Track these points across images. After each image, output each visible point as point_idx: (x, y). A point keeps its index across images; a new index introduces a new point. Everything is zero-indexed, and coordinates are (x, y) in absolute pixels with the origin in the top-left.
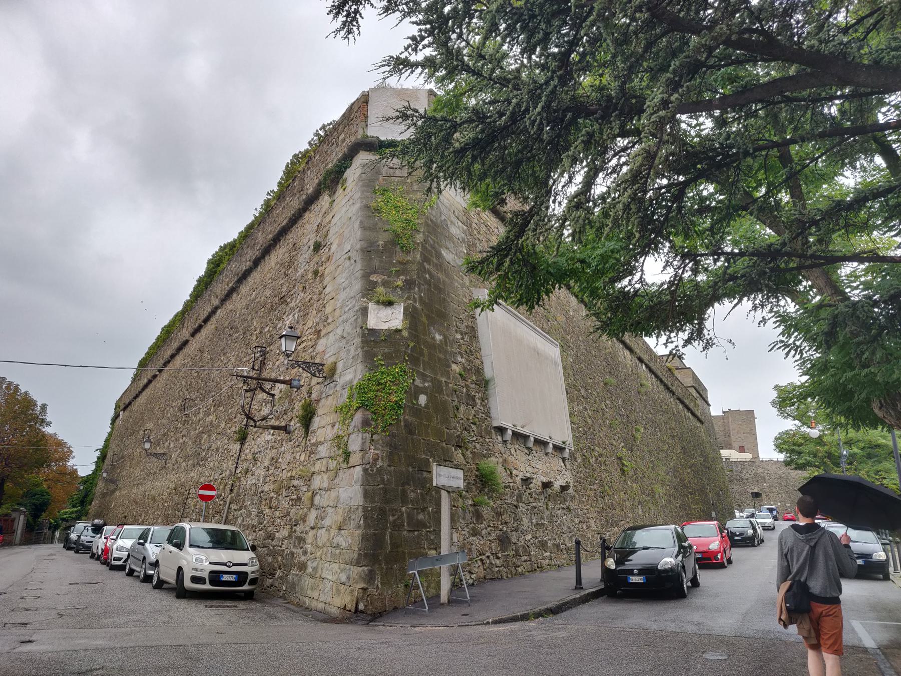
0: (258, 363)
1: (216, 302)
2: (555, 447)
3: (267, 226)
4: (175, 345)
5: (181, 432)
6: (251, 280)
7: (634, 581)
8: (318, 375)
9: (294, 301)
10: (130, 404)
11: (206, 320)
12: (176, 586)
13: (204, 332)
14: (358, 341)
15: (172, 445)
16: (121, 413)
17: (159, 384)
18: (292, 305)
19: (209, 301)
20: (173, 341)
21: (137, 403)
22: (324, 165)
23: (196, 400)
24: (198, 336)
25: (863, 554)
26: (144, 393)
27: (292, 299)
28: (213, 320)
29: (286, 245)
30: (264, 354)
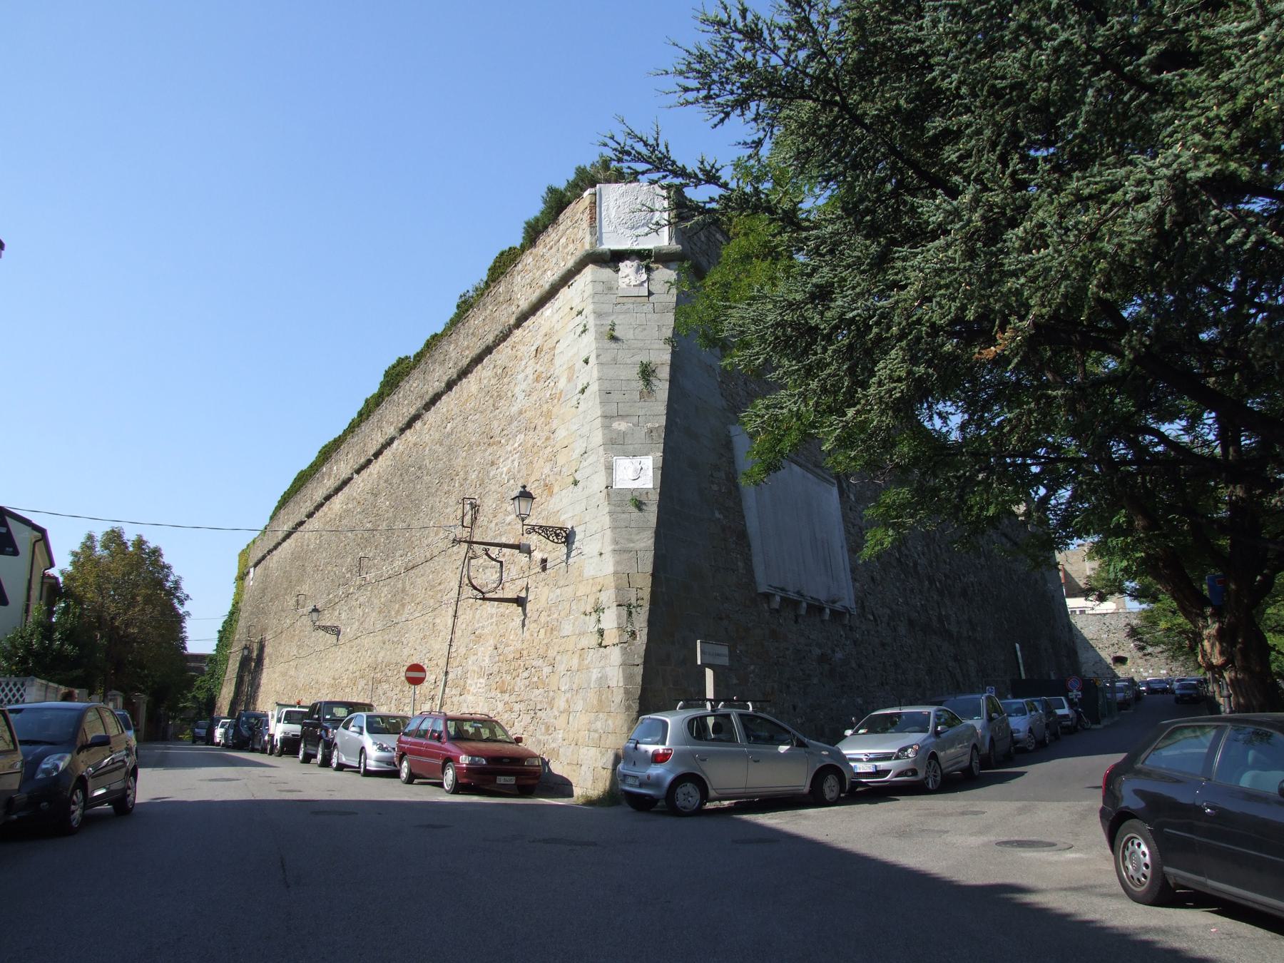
0: (468, 519)
1: (391, 431)
2: (834, 613)
3: (461, 338)
4: (329, 484)
5: (357, 600)
6: (442, 405)
7: (502, 782)
8: (556, 540)
9: (511, 442)
10: (264, 558)
11: (377, 454)
12: (90, 797)
13: (374, 468)
14: (605, 509)
15: (343, 616)
16: (252, 570)
17: (307, 535)
18: (509, 448)
19: (381, 428)
20: (326, 477)
21: (275, 558)
22: (540, 272)
23: (374, 559)
24: (365, 473)
25: (884, 730)
26: (285, 544)
27: (508, 441)
28: (387, 453)
29: (492, 366)
30: (474, 507)
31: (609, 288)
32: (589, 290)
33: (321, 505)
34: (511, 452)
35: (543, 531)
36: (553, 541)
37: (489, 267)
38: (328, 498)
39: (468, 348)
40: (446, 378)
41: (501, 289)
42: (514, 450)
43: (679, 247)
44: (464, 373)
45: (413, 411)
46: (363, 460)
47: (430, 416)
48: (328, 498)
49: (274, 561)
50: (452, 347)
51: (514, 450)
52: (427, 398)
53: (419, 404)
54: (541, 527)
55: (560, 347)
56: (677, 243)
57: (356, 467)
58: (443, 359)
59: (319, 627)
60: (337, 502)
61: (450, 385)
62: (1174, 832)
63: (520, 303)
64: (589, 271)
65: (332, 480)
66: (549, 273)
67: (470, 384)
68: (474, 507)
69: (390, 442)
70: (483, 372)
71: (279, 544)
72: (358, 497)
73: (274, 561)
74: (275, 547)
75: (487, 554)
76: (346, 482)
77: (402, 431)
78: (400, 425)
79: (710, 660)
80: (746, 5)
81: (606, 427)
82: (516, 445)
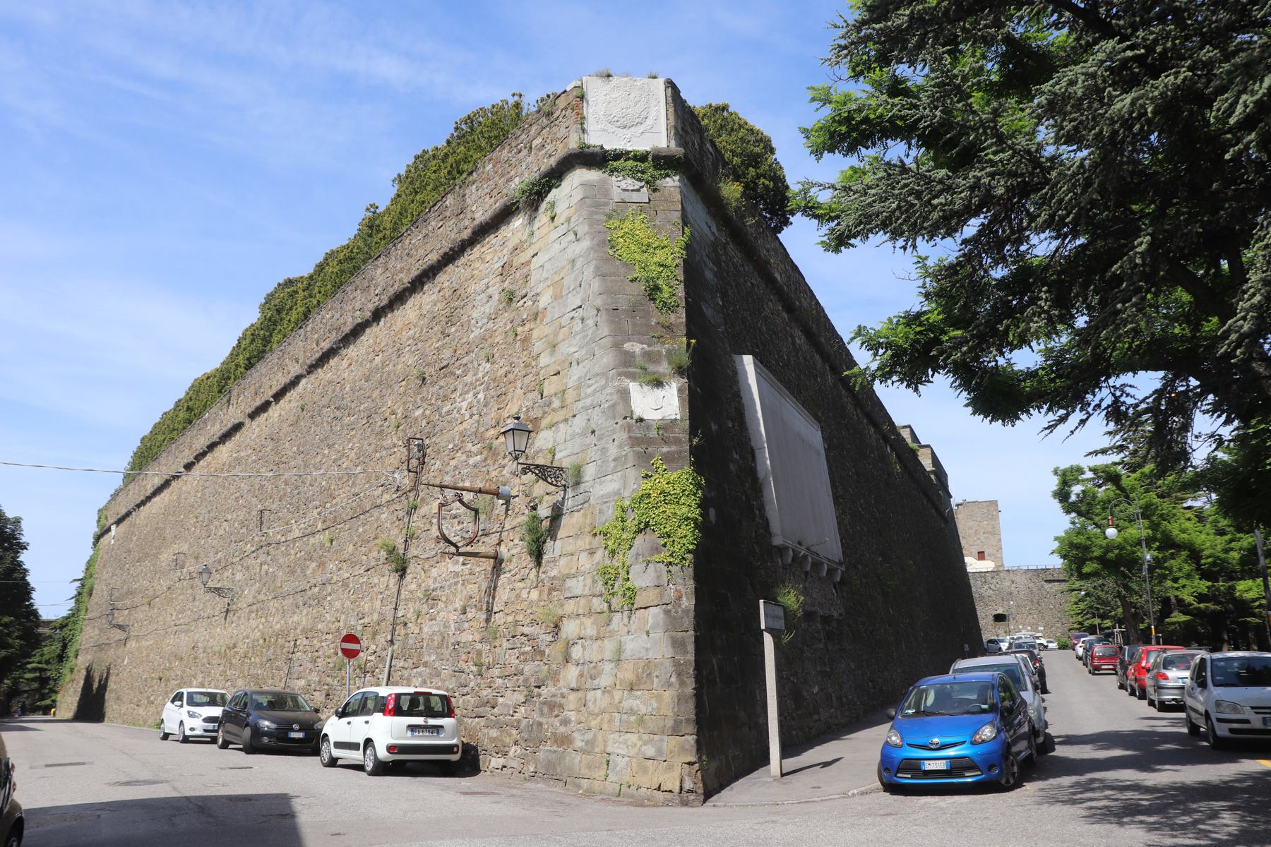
1: (296, 369)
8: (555, 483)
10: (128, 514)
11: (279, 396)
13: (274, 412)
16: (113, 527)
21: (143, 513)
26: (156, 499)
28: (292, 395)
31: (604, 190)
32: (578, 195)
33: (203, 454)
34: (471, 384)
35: (540, 471)
36: (551, 484)
37: (318, 262)
38: (212, 447)
39: (401, 271)
40: (371, 307)
41: (447, 202)
42: (477, 380)
43: (681, 151)
44: (399, 299)
45: (326, 345)
46: (258, 402)
47: (352, 351)
48: (212, 447)
49: (142, 518)
50: (379, 271)
51: (477, 380)
52: (347, 329)
53: (334, 337)
54: (538, 466)
55: (536, 262)
56: (679, 145)
57: (249, 410)
58: (366, 285)
59: (210, 588)
60: (223, 452)
61: (378, 314)
62: (955, 781)
63: (477, 215)
64: (579, 177)
65: (218, 426)
66: (517, 180)
67: (410, 311)
68: (421, 448)
69: (294, 383)
70: (427, 299)
71: (149, 499)
72: (252, 443)
73: (142, 518)
74: (143, 503)
75: (461, 501)
76: (238, 427)
77: (312, 368)
78: (309, 362)
79: (771, 625)
80: (391, 183)
81: (617, 346)
82: (480, 375)
